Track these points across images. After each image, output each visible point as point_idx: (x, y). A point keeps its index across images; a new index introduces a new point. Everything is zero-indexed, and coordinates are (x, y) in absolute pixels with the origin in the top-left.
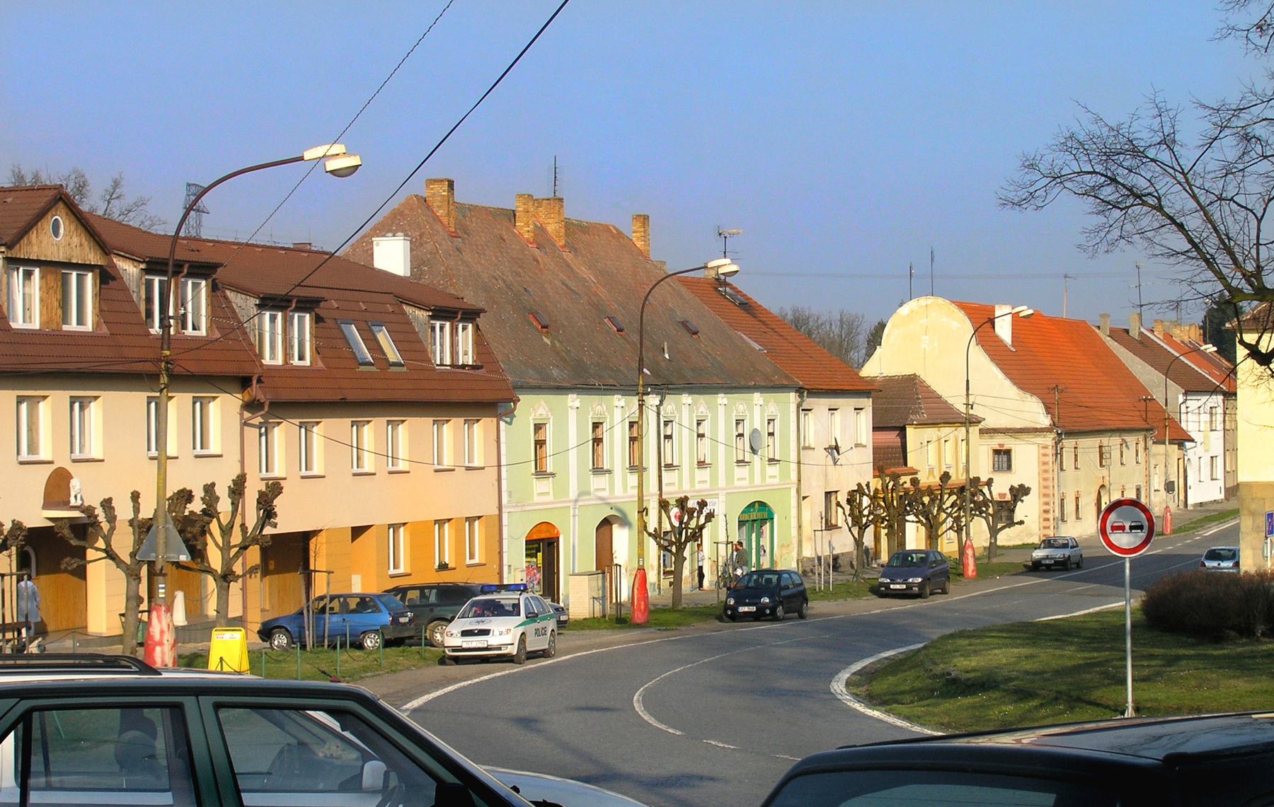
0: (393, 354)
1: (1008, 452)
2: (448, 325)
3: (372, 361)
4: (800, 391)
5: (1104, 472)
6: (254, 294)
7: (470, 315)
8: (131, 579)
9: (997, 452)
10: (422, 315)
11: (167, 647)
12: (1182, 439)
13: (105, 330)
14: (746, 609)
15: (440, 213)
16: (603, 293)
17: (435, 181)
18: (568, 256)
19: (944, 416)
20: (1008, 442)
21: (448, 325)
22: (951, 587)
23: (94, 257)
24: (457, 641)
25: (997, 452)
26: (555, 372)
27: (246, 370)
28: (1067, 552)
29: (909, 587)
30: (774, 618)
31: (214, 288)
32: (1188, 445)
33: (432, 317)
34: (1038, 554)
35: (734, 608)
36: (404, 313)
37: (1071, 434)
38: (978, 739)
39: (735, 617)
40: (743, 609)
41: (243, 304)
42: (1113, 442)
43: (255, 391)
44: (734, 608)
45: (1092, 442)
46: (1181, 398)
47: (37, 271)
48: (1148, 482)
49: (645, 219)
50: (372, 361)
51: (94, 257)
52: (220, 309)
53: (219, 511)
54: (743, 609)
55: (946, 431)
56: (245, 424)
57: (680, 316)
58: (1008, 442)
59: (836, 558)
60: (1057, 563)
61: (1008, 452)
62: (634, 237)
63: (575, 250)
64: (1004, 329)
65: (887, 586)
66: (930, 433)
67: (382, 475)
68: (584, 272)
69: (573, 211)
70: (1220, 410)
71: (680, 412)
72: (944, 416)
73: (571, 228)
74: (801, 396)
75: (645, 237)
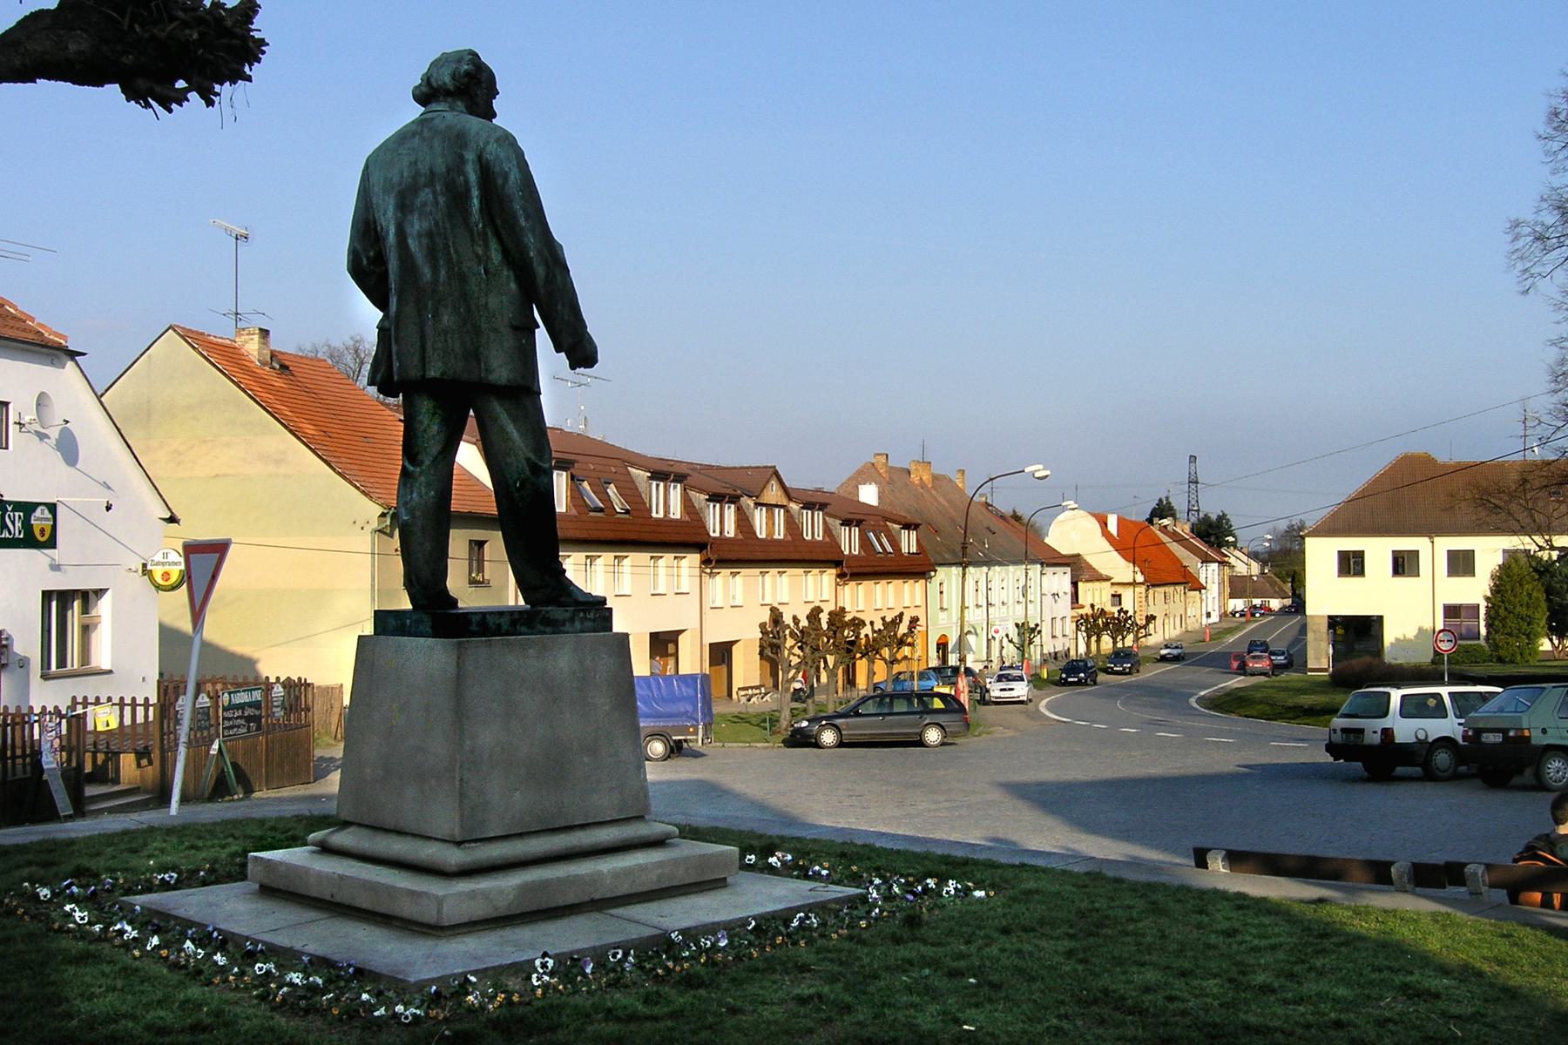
0: (889, 549)
1: (1120, 596)
2: (662, 484)
3: (601, 505)
4: (1042, 564)
5: (1166, 606)
6: (840, 518)
7: (916, 527)
8: (764, 662)
9: (1113, 596)
10: (897, 527)
11: (966, 693)
12: (1199, 588)
13: (789, 538)
14: (1072, 680)
15: (882, 471)
16: (952, 511)
17: (880, 454)
18: (933, 492)
19: (1099, 578)
20: (1120, 590)
21: (662, 484)
22: (1141, 668)
23: (785, 502)
24: (998, 693)
25: (1113, 596)
26: (947, 556)
27: (699, 539)
28: (1179, 651)
29: (1124, 669)
30: (1086, 684)
31: (685, 490)
32: (1203, 591)
33: (802, 508)
34: (1164, 652)
35: (1065, 679)
36: (629, 473)
37: (1153, 586)
38: (479, 883)
39: (1065, 683)
40: (1070, 680)
41: (699, 498)
42: (1170, 589)
43: (709, 553)
44: (1065, 679)
45: (1161, 590)
46: (1200, 565)
47: (764, 509)
48: (1186, 612)
49: (963, 472)
50: (601, 505)
51: (785, 502)
52: (687, 503)
53: (1431, 655)
54: (1070, 680)
55: (1097, 584)
56: (837, 584)
57: (986, 523)
58: (1120, 590)
59: (1056, 653)
60: (1174, 656)
61: (1120, 596)
62: (957, 481)
63: (935, 489)
64: (1113, 527)
65: (1112, 668)
66: (1089, 585)
67: (671, 595)
68: (941, 500)
69: (936, 470)
70: (1216, 572)
71: (1008, 575)
72: (1099, 578)
73: (935, 478)
74: (1042, 566)
75: (963, 482)
